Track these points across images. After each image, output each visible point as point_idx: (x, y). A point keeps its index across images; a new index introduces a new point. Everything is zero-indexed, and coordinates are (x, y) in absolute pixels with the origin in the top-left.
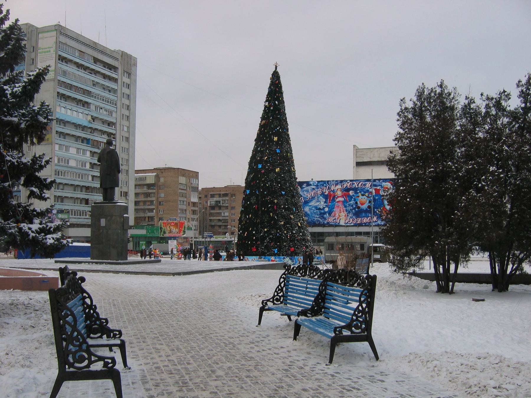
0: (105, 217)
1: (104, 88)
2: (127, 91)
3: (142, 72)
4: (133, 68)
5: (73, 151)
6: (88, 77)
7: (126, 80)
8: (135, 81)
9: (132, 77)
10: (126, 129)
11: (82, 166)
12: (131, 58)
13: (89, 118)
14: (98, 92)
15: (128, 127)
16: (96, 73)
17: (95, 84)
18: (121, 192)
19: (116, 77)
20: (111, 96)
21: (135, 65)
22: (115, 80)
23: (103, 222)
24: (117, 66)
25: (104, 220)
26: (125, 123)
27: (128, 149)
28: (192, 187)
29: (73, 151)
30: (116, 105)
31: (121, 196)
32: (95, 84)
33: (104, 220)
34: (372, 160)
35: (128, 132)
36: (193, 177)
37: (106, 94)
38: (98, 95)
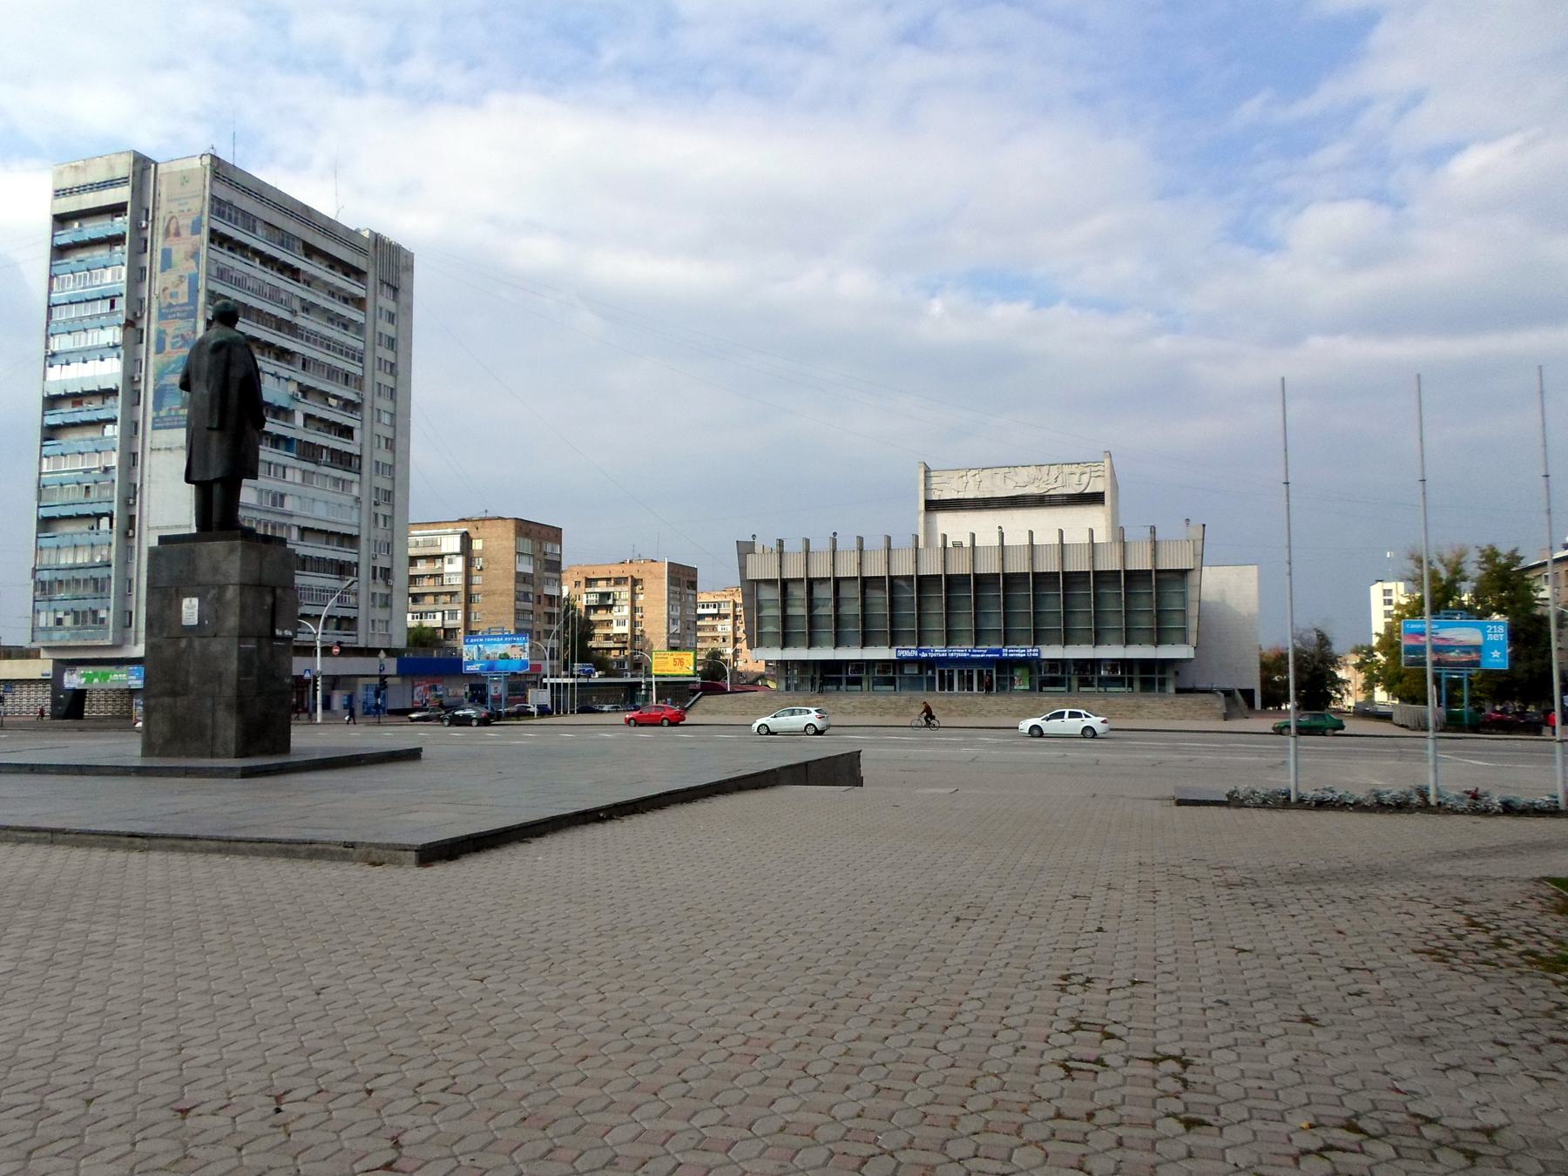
0: (198, 591)
1: (333, 318)
2: (389, 330)
3: (424, 285)
4: (403, 277)
5: (294, 476)
6: (291, 289)
7: (387, 303)
8: (410, 307)
9: (402, 296)
10: (386, 419)
11: (274, 504)
12: (398, 256)
13: (293, 388)
14: (313, 326)
15: (393, 415)
16: (310, 281)
17: (308, 307)
18: (374, 568)
19: (361, 293)
20: (349, 339)
21: (409, 268)
22: (359, 303)
23: (190, 609)
24: (363, 268)
25: (195, 601)
26: (384, 404)
27: (392, 467)
28: (547, 561)
29: (294, 476)
30: (361, 360)
31: (374, 577)
32: (308, 307)
33: (195, 601)
34: (961, 496)
35: (393, 425)
36: (549, 540)
37: (335, 333)
38: (316, 334)
